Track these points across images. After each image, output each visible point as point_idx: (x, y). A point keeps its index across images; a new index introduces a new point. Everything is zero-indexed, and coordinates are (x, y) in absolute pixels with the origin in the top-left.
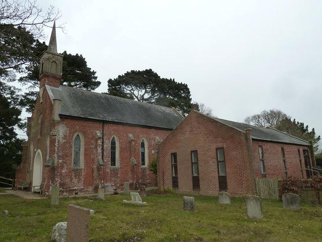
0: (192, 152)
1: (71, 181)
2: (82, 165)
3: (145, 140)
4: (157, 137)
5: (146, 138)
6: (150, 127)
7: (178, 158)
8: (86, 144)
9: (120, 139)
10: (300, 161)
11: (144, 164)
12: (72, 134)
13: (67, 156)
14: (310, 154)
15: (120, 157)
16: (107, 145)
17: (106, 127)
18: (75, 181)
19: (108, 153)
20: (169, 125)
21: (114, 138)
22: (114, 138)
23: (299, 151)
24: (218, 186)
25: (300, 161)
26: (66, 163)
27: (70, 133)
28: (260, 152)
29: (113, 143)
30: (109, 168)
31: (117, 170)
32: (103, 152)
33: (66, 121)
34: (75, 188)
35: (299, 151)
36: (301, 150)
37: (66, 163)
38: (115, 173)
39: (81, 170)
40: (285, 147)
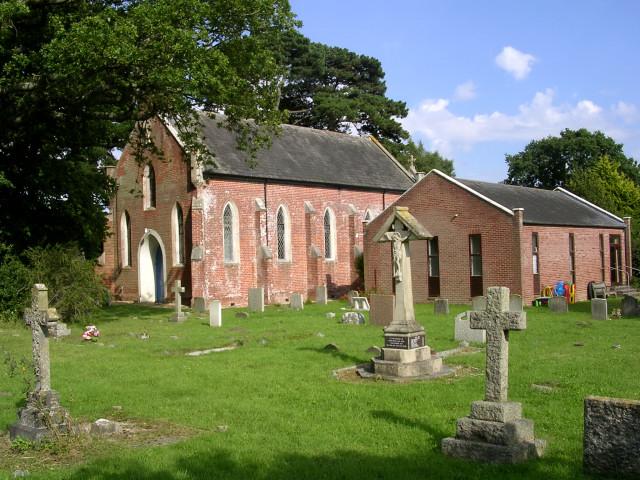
0: (470, 236)
1: (224, 283)
2: (237, 259)
3: (284, 209)
4: (351, 205)
5: (331, 207)
6: (339, 187)
7: (441, 246)
8: (243, 221)
9: (291, 210)
10: (602, 254)
11: (328, 255)
12: (220, 203)
13: (217, 244)
14: (623, 241)
15: (293, 242)
16: (273, 223)
17: (271, 188)
18: (229, 284)
19: (273, 236)
20: (372, 180)
21: (228, 206)
22: (228, 206)
23: (601, 236)
24: (469, 291)
25: (602, 254)
26: (215, 255)
27: (219, 203)
29: (280, 217)
30: (275, 263)
31: (331, 263)
32: (267, 236)
34: (230, 296)
35: (601, 236)
36: (606, 234)
37: (215, 255)
38: (285, 268)
39: (236, 266)
40: (577, 232)
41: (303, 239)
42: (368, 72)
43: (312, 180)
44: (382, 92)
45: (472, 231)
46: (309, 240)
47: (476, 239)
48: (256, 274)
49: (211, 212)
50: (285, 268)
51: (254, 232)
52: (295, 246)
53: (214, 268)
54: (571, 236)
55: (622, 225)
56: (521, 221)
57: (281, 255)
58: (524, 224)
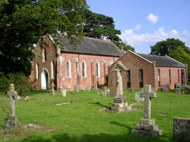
0: (140, 70)
1: (66, 84)
2: (70, 77)
3: (84, 62)
4: (104, 61)
6: (101, 55)
7: (131, 73)
8: (72, 65)
9: (86, 62)
10: (179, 75)
11: (97, 75)
12: (65, 60)
13: (64, 72)
14: (185, 71)
15: (87, 72)
16: (81, 66)
17: (80, 56)
18: (68, 84)
19: (81, 70)
20: (110, 53)
21: (68, 61)
22: (68, 61)
23: (178, 70)
24: (139, 86)
25: (179, 75)
26: (64, 75)
27: (65, 60)
28: (159, 78)
29: (83, 64)
30: (82, 78)
31: (98, 78)
32: (79, 70)
33: (63, 54)
34: (68, 87)
35: (178, 70)
36: (180, 69)
37: (64, 75)
38: (85, 79)
39: (70, 79)
40: (171, 69)
41: (90, 71)
42: (109, 21)
43: (93, 53)
44: (113, 27)
45: (140, 68)
46: (92, 71)
47: (141, 71)
48: (76, 81)
49: (63, 63)
50: (85, 79)
51: (75, 69)
52: (88, 73)
53: (63, 79)
54: (170, 70)
55: (185, 67)
56: (155, 65)
57: (84, 76)
58: (156, 66)
